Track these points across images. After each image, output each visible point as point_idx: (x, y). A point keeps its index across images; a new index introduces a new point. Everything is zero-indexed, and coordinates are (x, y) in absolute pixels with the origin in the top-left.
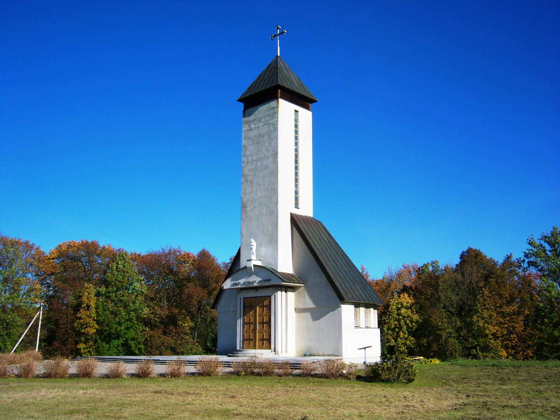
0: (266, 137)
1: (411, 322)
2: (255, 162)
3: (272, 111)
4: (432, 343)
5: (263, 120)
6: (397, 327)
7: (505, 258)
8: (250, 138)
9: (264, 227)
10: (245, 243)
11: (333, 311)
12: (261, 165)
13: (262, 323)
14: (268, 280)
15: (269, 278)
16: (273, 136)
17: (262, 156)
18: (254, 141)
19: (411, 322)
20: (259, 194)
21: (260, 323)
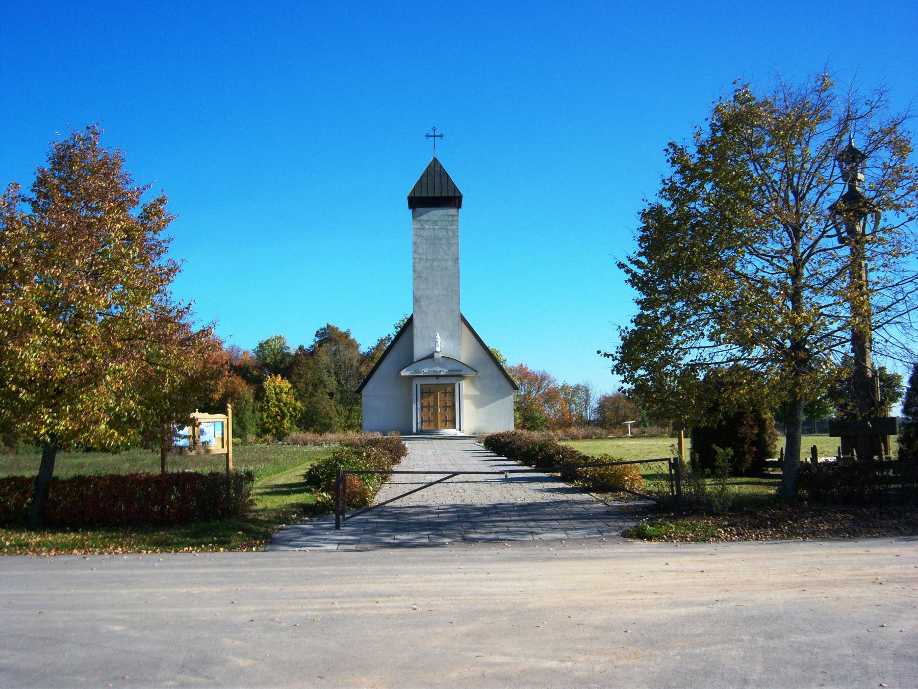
0: (443, 241)
1: (295, 410)
2: (431, 262)
3: (450, 218)
4: (13, 442)
5: (439, 223)
6: (279, 415)
7: (195, 329)
8: (422, 237)
9: (443, 322)
10: (419, 335)
11: (503, 398)
12: (438, 266)
13: (445, 407)
14: (459, 371)
15: (459, 369)
16: (452, 241)
17: (439, 257)
18: (428, 241)
19: (295, 410)
20: (436, 292)
21: (442, 407)
